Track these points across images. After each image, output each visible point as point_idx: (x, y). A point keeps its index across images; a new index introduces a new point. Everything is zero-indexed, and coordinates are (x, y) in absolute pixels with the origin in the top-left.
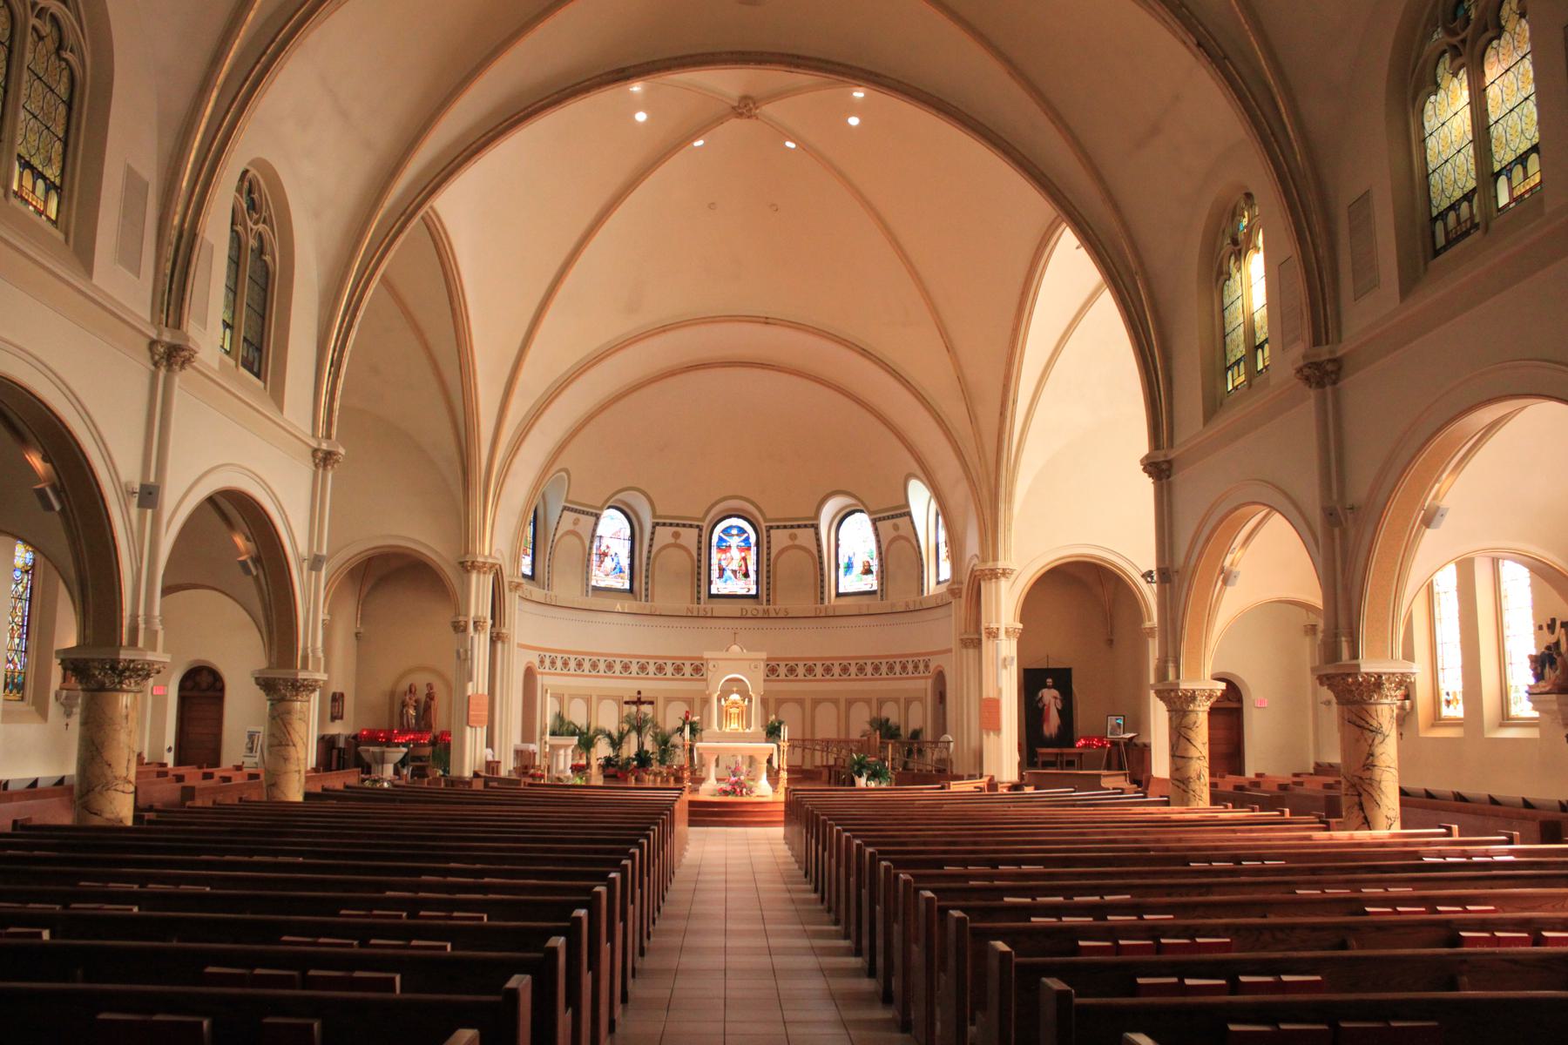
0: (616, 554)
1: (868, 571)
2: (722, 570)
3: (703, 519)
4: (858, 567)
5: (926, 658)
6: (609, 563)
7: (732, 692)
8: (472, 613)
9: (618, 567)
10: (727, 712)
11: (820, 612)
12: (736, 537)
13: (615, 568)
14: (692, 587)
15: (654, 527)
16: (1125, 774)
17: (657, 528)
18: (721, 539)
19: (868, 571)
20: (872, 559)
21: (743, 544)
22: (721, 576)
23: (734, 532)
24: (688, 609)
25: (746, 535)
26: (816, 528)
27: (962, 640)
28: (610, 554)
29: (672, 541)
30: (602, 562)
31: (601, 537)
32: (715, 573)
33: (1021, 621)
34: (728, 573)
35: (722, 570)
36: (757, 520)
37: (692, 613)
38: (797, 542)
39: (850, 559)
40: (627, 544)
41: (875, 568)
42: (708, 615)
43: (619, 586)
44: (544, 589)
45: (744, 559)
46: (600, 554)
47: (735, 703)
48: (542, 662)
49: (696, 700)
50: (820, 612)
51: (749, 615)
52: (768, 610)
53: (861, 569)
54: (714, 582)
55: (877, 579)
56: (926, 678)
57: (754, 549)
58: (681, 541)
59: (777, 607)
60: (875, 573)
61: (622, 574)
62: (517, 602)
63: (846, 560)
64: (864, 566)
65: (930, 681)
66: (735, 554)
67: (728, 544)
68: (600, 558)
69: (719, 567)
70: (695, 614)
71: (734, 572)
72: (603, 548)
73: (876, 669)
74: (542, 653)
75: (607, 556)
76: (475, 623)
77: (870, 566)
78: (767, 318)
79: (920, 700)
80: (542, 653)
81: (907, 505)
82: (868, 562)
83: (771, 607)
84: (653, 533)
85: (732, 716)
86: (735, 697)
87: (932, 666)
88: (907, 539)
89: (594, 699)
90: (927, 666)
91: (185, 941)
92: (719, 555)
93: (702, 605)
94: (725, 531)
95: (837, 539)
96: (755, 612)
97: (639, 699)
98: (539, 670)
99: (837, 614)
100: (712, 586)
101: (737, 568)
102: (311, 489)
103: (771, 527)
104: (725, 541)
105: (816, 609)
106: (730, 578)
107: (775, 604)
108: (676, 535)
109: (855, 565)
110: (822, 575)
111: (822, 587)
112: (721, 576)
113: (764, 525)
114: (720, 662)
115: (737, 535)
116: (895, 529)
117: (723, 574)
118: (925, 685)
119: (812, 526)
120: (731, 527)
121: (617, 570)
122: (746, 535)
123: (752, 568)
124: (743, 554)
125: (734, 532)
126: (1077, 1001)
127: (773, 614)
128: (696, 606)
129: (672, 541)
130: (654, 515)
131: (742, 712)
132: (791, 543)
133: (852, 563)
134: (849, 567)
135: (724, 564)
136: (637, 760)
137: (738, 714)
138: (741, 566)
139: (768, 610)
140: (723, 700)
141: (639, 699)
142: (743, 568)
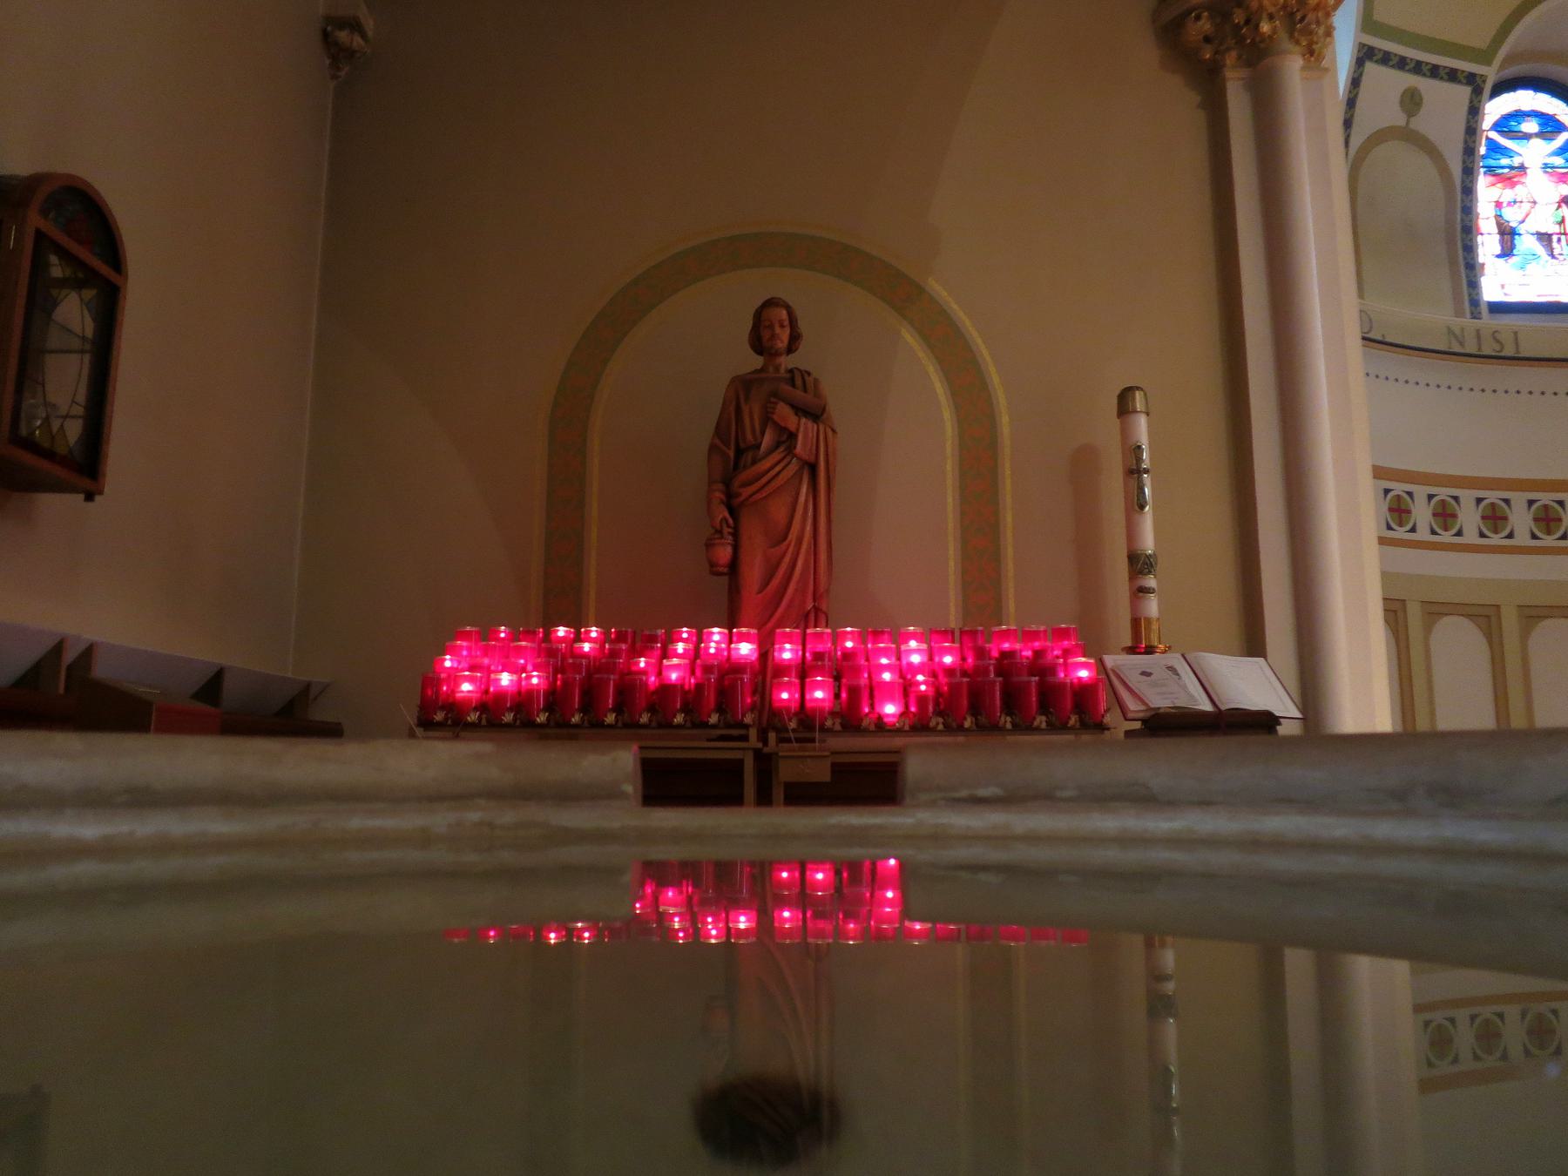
2: (1508, 235)
12: (1536, 142)
14: (1454, 274)
15: (1360, 62)
21: (1559, 161)
22: (1507, 251)
23: (1531, 126)
32: (1488, 245)
34: (1526, 243)
35: (1508, 235)
37: (1462, 344)
49: (1409, 605)
67: (1516, 161)
70: (1471, 348)
84: (1355, 82)
89: (1510, 621)
91: (68, 677)
102: (40, 736)
104: (1504, 151)
112: (1507, 251)
115: (1540, 135)
117: (1513, 247)
120: (1519, 115)
125: (1531, 126)
126: (584, 674)
128: (1467, 321)
129: (1399, 119)
135: (1512, 216)
136: (910, 680)
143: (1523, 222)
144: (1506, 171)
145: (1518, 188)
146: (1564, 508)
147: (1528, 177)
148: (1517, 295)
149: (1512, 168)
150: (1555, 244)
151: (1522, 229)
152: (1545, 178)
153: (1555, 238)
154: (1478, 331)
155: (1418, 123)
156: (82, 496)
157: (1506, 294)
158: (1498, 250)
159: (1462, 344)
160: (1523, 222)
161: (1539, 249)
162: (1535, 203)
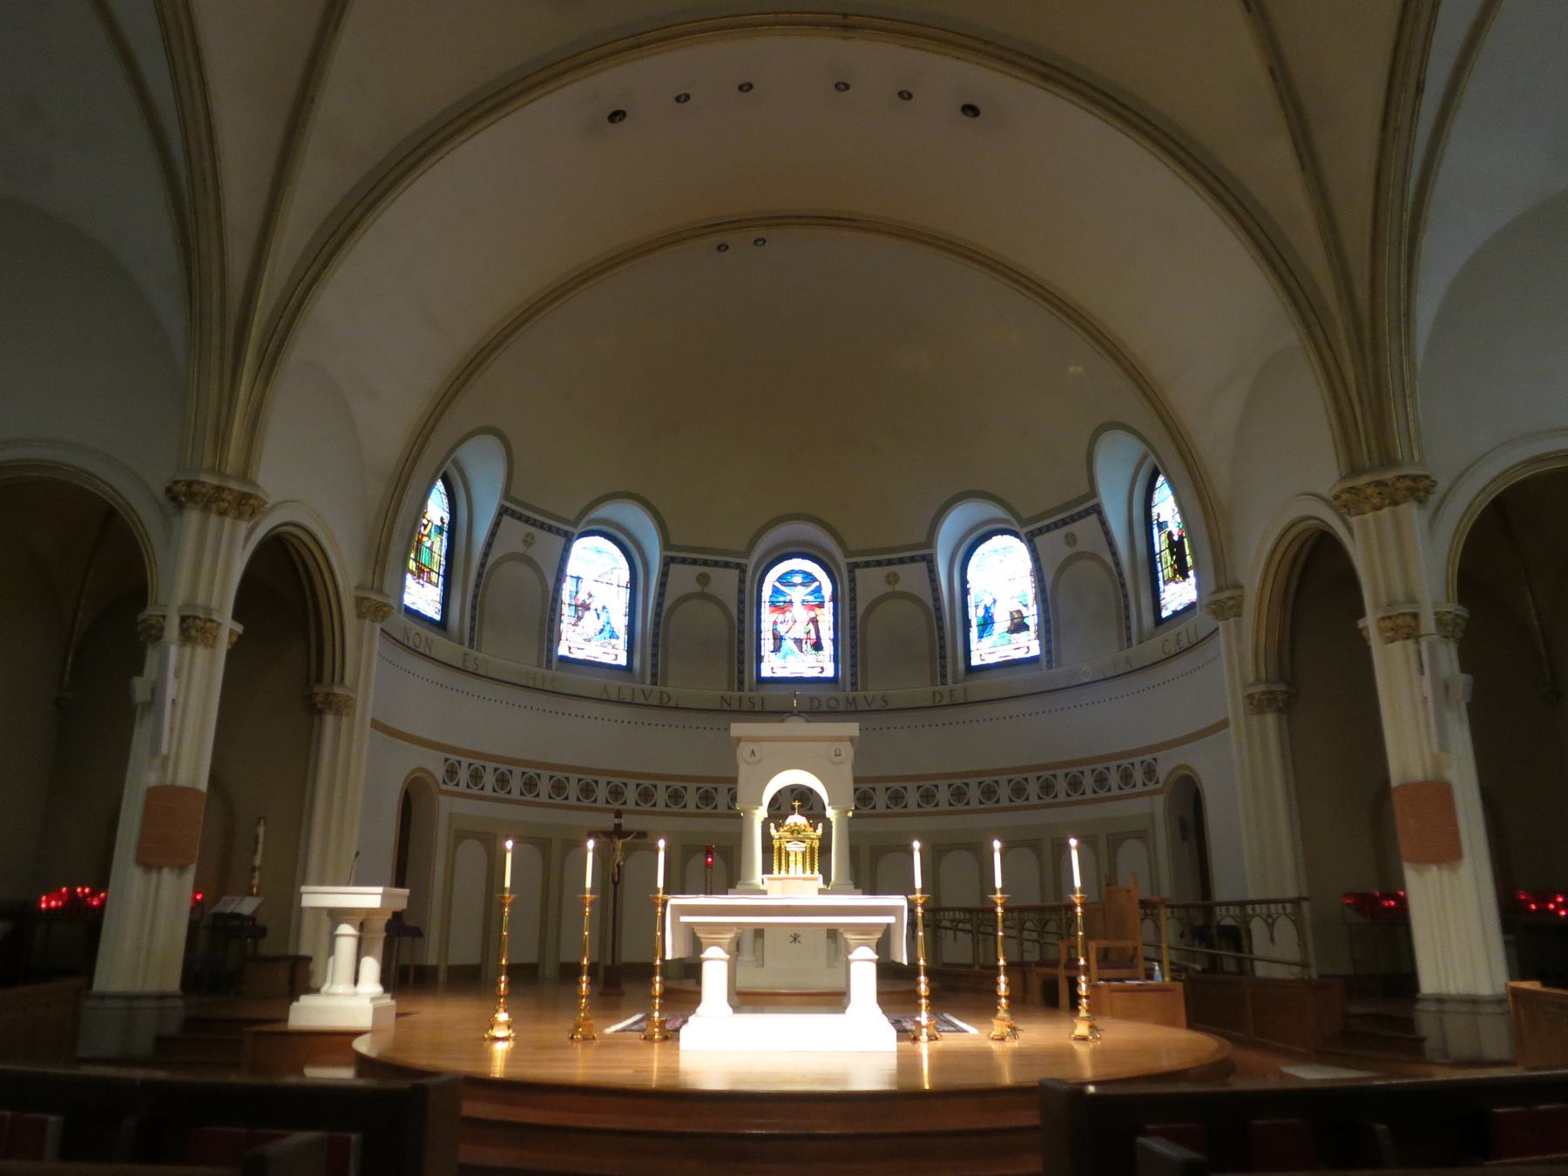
0: (604, 608)
1: (1018, 626)
2: (778, 639)
3: (747, 553)
4: (1002, 622)
5: (1148, 758)
6: (590, 621)
7: (792, 810)
8: (180, 595)
9: (608, 628)
10: (780, 848)
11: (942, 698)
12: (799, 587)
13: (601, 631)
16: (1304, 965)
17: (672, 566)
18: (776, 591)
19: (1018, 626)
20: (1026, 606)
21: (811, 598)
22: (777, 649)
23: (798, 579)
24: (722, 697)
25: (817, 584)
26: (930, 561)
27: (1250, 697)
28: (593, 607)
29: (696, 588)
30: (579, 618)
31: (578, 578)
32: (767, 644)
33: (1462, 601)
34: (788, 645)
35: (778, 639)
36: (833, 559)
37: (730, 705)
38: (899, 587)
39: (987, 609)
40: (624, 595)
41: (1032, 621)
42: (756, 709)
43: (608, 660)
44: (461, 643)
45: (814, 621)
46: (576, 606)
47: (795, 832)
48: (452, 772)
50: (942, 698)
51: (824, 708)
52: (854, 699)
53: (1009, 624)
54: (766, 659)
55: (1038, 637)
56: (1152, 793)
57: (829, 606)
58: (712, 589)
59: (869, 694)
60: (1033, 628)
61: (613, 641)
62: (377, 644)
63: (981, 612)
64: (1012, 619)
65: (1159, 802)
66: (800, 614)
67: (788, 599)
68: (576, 611)
69: (774, 634)
70: (735, 707)
71: (798, 642)
72: (582, 597)
73: (1047, 787)
74: (453, 758)
75: (588, 609)
76: (184, 619)
77: (1022, 617)
78: (846, 16)
79: (1143, 835)
80: (453, 758)
81: (1093, 492)
82: (1019, 612)
83: (860, 694)
85: (792, 858)
86: (796, 820)
87: (1162, 772)
88: (1093, 557)
90: (1150, 772)
92: (774, 616)
93: (747, 693)
94: (783, 579)
95: (964, 582)
96: (833, 703)
97: (618, 826)
98: (443, 787)
99: (971, 699)
100: (763, 665)
101: (802, 636)
103: (857, 565)
104: (782, 593)
105: (934, 693)
106: (792, 652)
107: (865, 688)
108: (703, 579)
109: (996, 619)
110: (942, 638)
111: (943, 657)
112: (777, 649)
113: (842, 562)
114: (766, 745)
115: (803, 584)
116: (1068, 544)
118: (1154, 808)
119: (924, 558)
120: (792, 573)
121: (606, 634)
122: (817, 584)
123: (827, 635)
124: (812, 614)
125: (798, 579)
127: (862, 706)
130: (666, 543)
131: (812, 849)
132: (889, 589)
133: (992, 617)
134: (987, 623)
135: (782, 629)
137: (804, 854)
138: (808, 633)
139: (854, 699)
140: (772, 825)
141: (618, 826)
142: (813, 636)
143: (787, 632)
144: (782, 604)
145: (788, 614)
146: (716, 792)
147: (970, 583)
148: (780, 673)
149: (785, 602)
150: (804, 645)
151: (786, 636)
152: (802, 608)
153: (804, 641)
154: (740, 698)
155: (708, 590)
156: (613, 815)
157: (982, 660)
158: (772, 648)
159: (730, 705)
160: (787, 632)
161: (795, 648)
162: (795, 621)
